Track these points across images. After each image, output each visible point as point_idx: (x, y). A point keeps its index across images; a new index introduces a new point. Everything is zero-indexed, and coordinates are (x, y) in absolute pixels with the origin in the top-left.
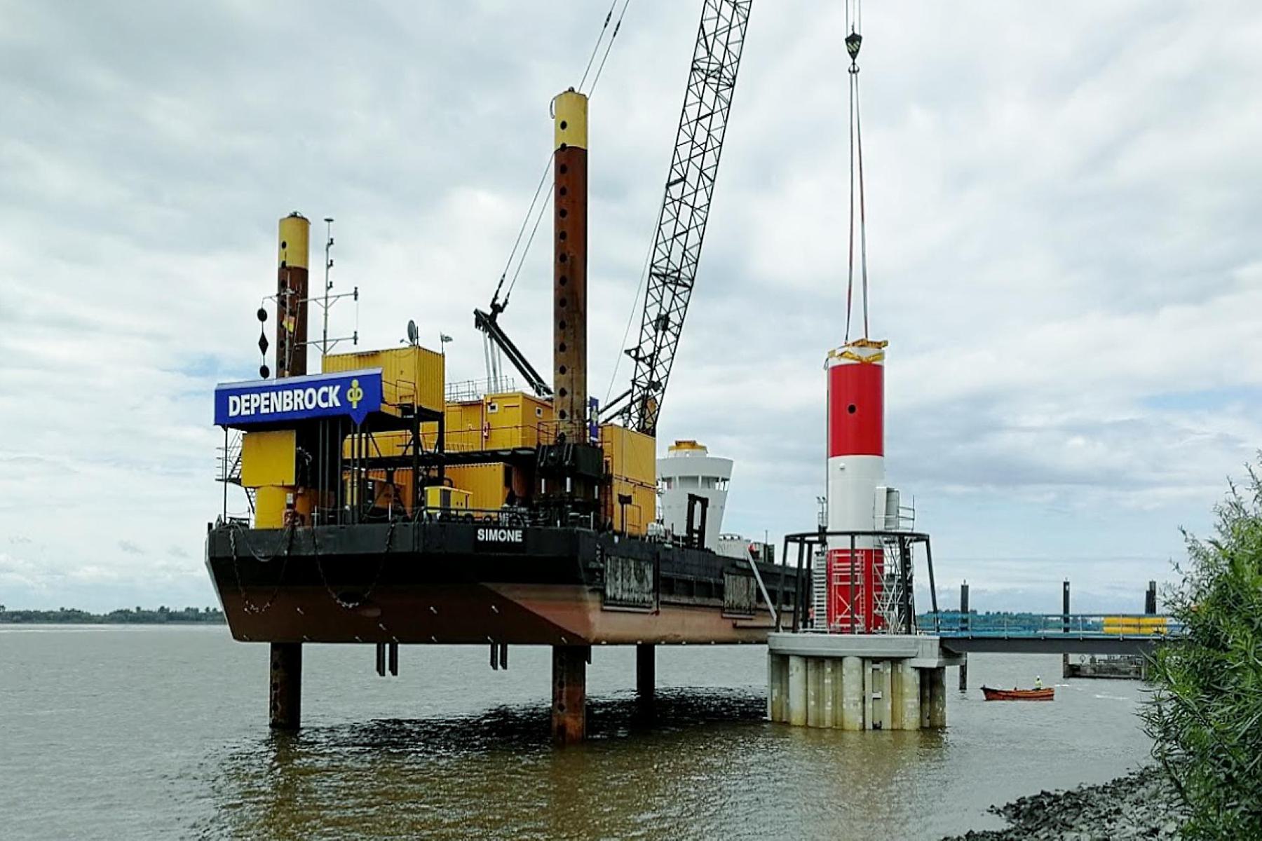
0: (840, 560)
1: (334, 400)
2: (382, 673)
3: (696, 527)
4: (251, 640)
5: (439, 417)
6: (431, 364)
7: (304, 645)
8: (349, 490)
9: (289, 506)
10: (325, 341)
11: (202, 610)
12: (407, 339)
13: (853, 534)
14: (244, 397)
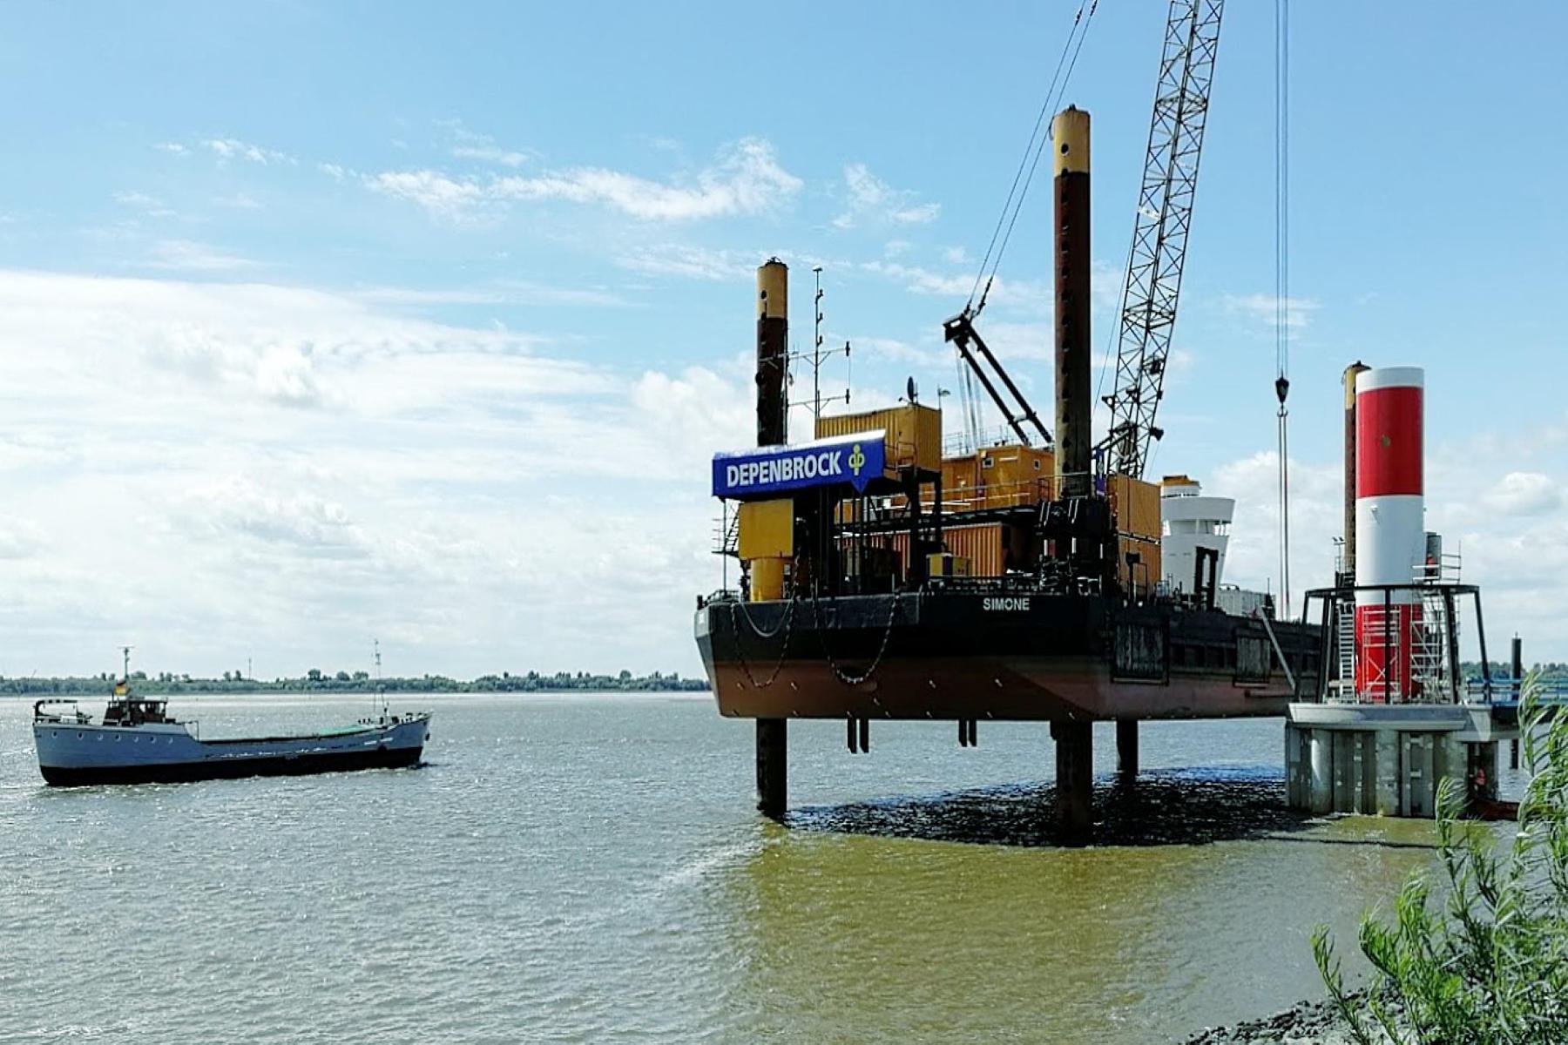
0: (1372, 618)
1: (834, 467)
2: (854, 751)
3: (1205, 585)
4: (738, 715)
5: (936, 478)
6: (927, 422)
7: (1094, 724)
8: (850, 561)
9: (787, 578)
10: (817, 401)
11: (574, 676)
12: (906, 397)
13: (1388, 589)
14: (743, 467)
